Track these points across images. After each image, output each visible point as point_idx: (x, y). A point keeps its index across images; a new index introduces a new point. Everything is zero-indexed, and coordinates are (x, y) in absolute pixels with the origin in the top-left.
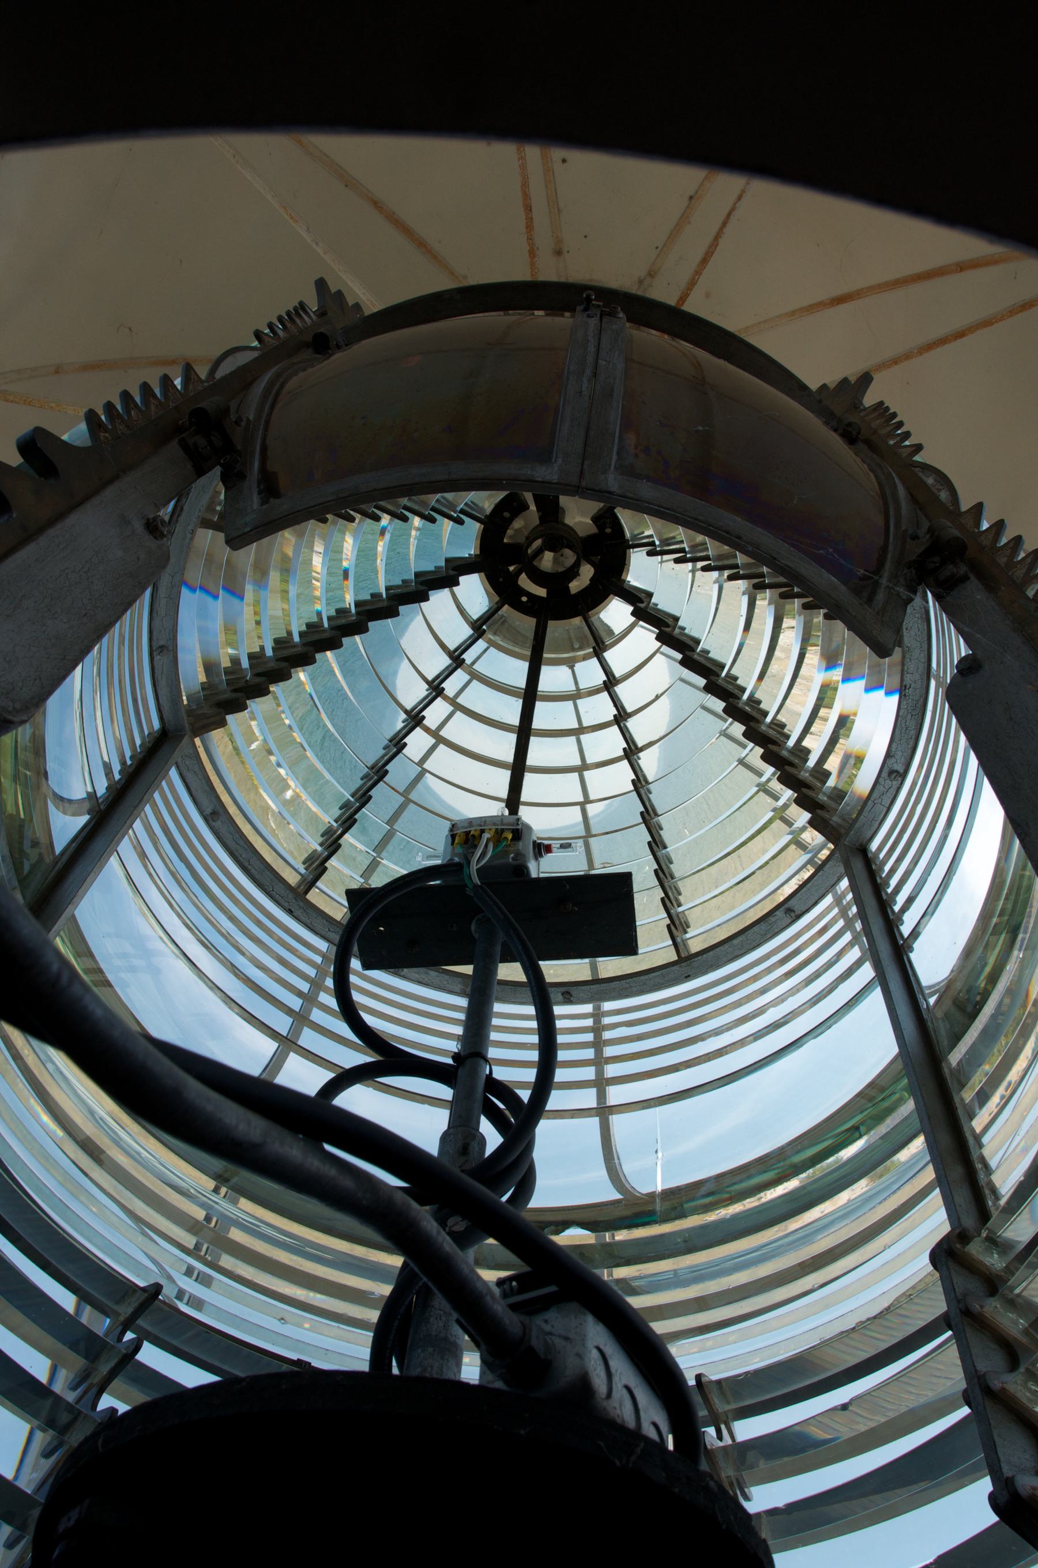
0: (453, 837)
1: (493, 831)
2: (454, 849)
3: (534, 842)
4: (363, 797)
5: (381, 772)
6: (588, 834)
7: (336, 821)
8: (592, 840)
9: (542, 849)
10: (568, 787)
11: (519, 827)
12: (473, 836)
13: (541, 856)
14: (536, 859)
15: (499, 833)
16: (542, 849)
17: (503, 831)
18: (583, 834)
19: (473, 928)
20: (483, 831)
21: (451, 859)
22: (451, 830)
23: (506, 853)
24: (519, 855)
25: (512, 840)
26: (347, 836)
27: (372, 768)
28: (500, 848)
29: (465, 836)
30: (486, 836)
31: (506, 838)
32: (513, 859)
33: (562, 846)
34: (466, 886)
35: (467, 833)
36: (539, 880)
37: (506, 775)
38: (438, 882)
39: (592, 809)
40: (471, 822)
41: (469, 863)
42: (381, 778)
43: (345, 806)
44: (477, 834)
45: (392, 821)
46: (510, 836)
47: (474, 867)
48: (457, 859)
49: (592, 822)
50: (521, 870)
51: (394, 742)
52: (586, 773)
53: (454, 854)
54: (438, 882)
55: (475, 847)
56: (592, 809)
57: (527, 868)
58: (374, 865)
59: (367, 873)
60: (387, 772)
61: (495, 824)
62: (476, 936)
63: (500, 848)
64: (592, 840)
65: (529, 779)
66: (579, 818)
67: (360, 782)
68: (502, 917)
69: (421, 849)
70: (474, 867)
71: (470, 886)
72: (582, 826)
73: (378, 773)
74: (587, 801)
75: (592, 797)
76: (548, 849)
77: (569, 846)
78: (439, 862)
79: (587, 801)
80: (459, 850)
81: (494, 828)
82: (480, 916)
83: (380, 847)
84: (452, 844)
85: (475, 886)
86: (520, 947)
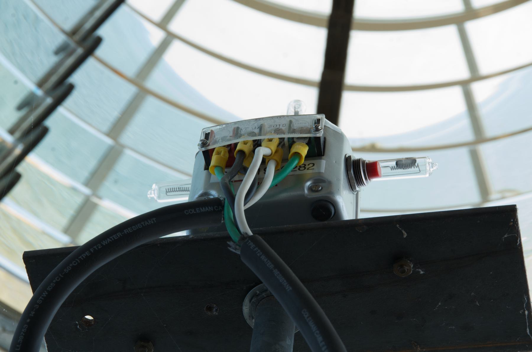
0: (207, 155)
1: (276, 142)
2: (209, 175)
3: (348, 159)
4: (60, 88)
5: (89, 42)
6: (480, 137)
7: (11, 132)
8: (485, 149)
9: (360, 171)
10: (438, 54)
11: (320, 134)
12: (242, 152)
13: (360, 182)
14: (352, 188)
15: (286, 146)
16: (360, 171)
17: (292, 142)
18: (468, 136)
19: (246, 309)
20: (257, 144)
21: (205, 194)
22: (204, 144)
23: (299, 180)
24: (320, 182)
25: (307, 157)
26: (32, 158)
27: (72, 33)
28: (288, 171)
29: (227, 155)
30: (262, 151)
31: (297, 155)
32: (310, 189)
33: (400, 164)
34: (229, 238)
35: (231, 148)
36: (356, 224)
37: (319, 37)
38: (183, 233)
39: (481, 91)
40: (237, 129)
41: (232, 198)
42: (90, 52)
43: (28, 103)
44: (247, 149)
45: (116, 129)
46: (304, 151)
47: (241, 207)
48: (214, 194)
49: (483, 112)
50: (325, 208)
51: (78, 37)
52: (471, 26)
53: (209, 185)
54: (183, 233)
55: (244, 170)
56: (481, 91)
57: (335, 205)
58: (86, 210)
59: (71, 229)
60: (98, 41)
61: (278, 131)
62: (252, 323)
63: (288, 171)
64: (485, 149)
65: (358, 42)
66: (461, 107)
67: (54, 60)
68: (289, 288)
69: (160, 177)
70: (241, 207)
71: (235, 237)
72: (466, 122)
73: (85, 42)
74: (476, 76)
75: (484, 69)
76: (372, 170)
77: (412, 163)
78: (184, 199)
79: (476, 76)
80: (217, 177)
81: (276, 137)
82: (256, 289)
83: (96, 178)
84: (207, 168)
85: (244, 237)
86: (320, 339)
